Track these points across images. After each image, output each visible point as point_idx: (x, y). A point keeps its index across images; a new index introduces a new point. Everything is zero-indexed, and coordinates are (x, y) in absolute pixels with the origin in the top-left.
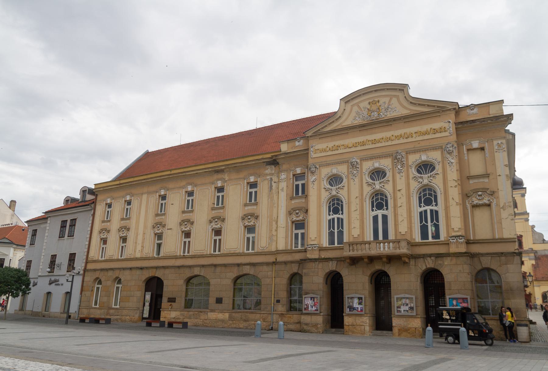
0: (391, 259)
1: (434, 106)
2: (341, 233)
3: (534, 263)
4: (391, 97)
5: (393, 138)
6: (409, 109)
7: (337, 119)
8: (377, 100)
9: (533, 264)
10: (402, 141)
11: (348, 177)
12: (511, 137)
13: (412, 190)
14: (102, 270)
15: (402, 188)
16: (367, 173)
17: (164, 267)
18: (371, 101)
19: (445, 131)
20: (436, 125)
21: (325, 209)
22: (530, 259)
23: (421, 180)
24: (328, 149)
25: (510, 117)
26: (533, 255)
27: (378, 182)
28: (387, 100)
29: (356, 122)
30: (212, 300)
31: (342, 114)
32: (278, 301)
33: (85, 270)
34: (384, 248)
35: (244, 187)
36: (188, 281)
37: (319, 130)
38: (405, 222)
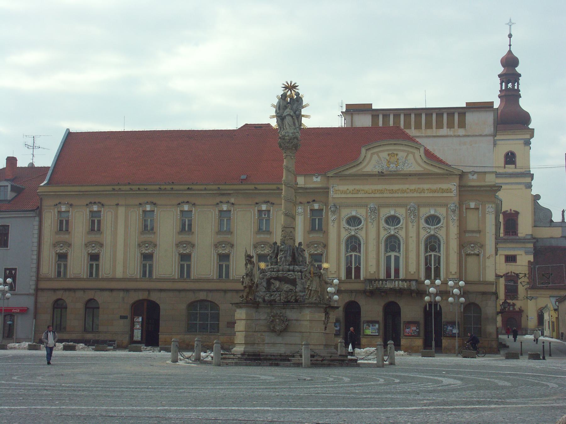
0: (400, 292)
1: (444, 169)
2: (358, 269)
3: (532, 260)
4: (409, 153)
5: (408, 191)
6: (422, 167)
7: (358, 164)
8: (395, 152)
9: (529, 262)
10: (415, 195)
11: (366, 220)
12: (499, 202)
14: (65, 290)
15: (412, 236)
16: (424, 218)
17: (161, 290)
18: (390, 152)
19: (451, 192)
20: (445, 186)
21: (343, 247)
22: (527, 253)
24: (348, 192)
26: (531, 245)
27: (393, 228)
31: (363, 160)
33: (37, 290)
34: (186, 228)
36: (192, 305)
38: (412, 263)
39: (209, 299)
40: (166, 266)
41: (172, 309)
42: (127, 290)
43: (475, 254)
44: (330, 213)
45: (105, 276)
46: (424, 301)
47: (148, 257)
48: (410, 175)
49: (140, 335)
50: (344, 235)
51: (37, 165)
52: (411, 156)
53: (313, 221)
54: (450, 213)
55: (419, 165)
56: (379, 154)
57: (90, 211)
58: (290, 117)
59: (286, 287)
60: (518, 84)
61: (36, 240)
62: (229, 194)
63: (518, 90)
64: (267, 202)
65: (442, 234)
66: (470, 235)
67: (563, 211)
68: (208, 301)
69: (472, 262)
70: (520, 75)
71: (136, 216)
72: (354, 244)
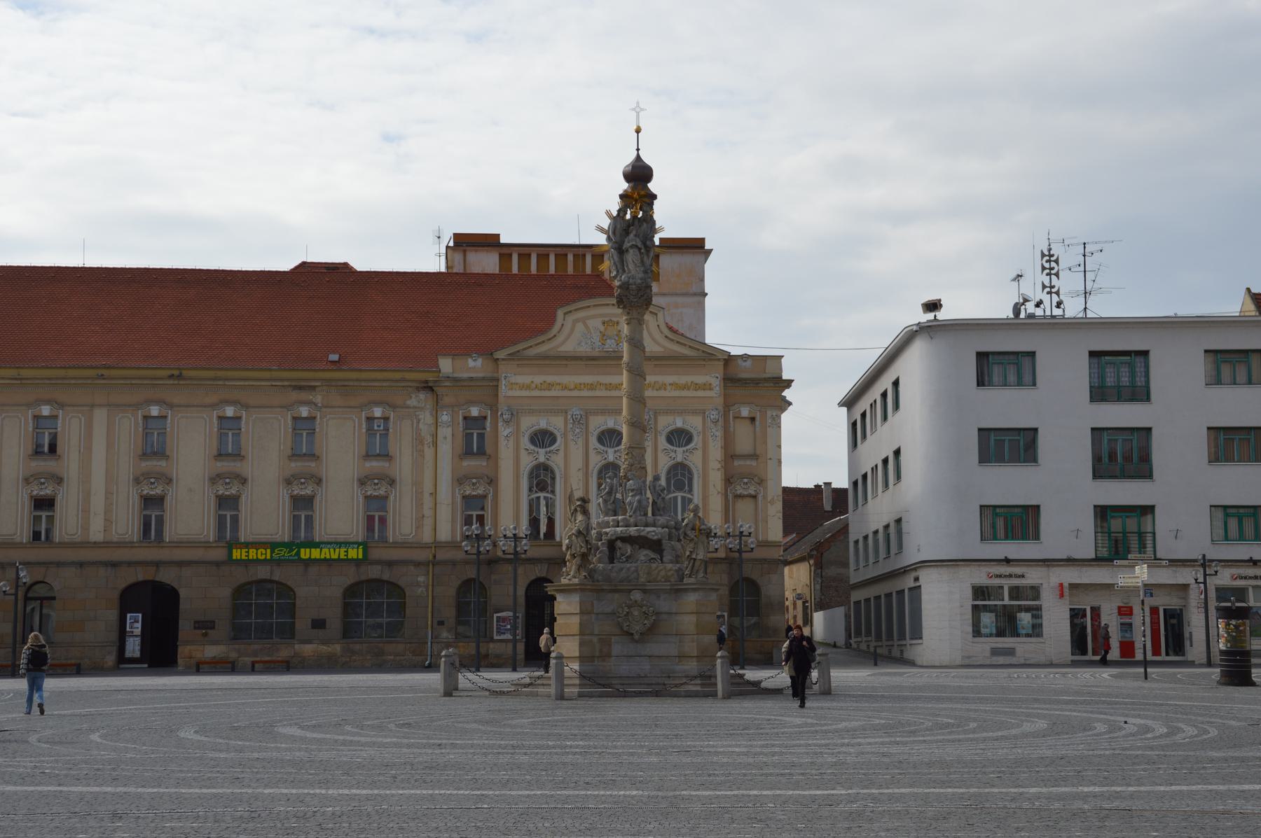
2: (160, 532)
8: (615, 319)
11: (565, 435)
13: (660, 467)
16: (596, 433)
17: (181, 564)
19: (711, 389)
20: (700, 379)
23: (673, 455)
25: (789, 383)
29: (581, 349)
30: (302, 624)
32: (441, 623)
34: (228, 448)
35: (360, 425)
39: (276, 578)
40: (190, 517)
41: (200, 596)
42: (114, 565)
44: (500, 424)
45: (67, 539)
47: (44, 504)
49: (138, 648)
50: (527, 463)
53: (468, 437)
54: (709, 423)
56: (588, 322)
57: (220, 418)
62: (313, 388)
64: (48, 402)
65: (695, 461)
66: (741, 462)
68: (271, 581)
69: (744, 507)
70: (654, 197)
71: (128, 427)
72: (542, 478)
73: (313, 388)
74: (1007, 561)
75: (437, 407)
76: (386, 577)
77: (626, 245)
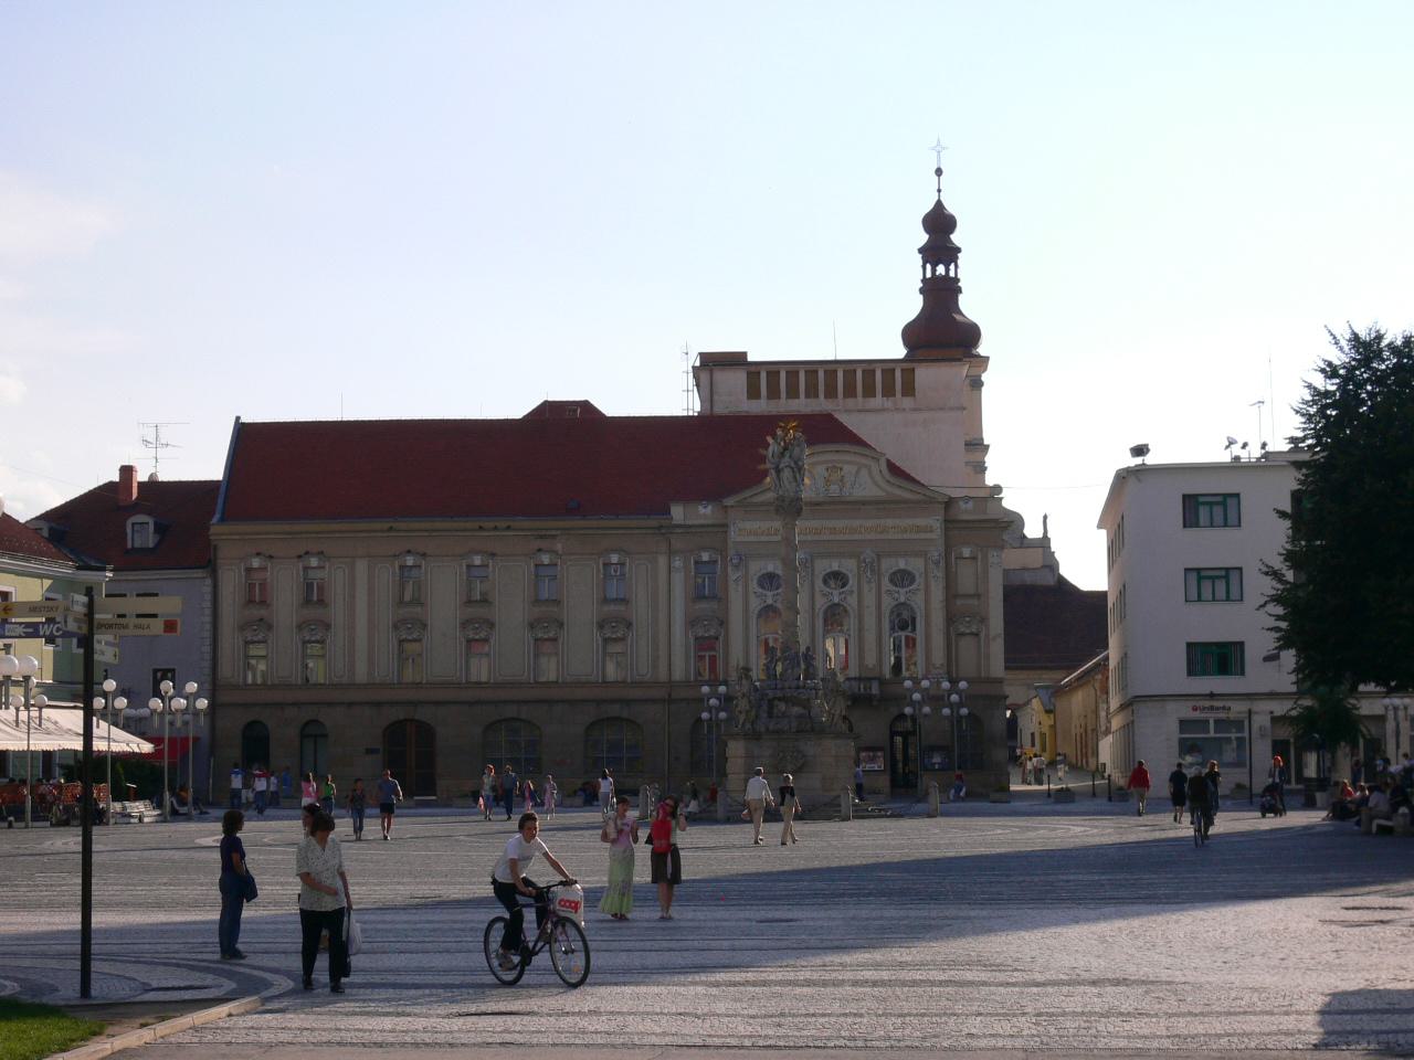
13: (883, 608)
17: (437, 703)
19: (931, 531)
20: (921, 522)
23: (896, 595)
28: (853, 469)
35: (598, 571)
37: (745, 499)
42: (378, 704)
43: (972, 634)
44: (730, 569)
46: (700, 691)
48: (864, 503)
51: (163, 477)
52: (864, 472)
55: (879, 486)
58: (789, 469)
59: (796, 710)
60: (956, 267)
61: (208, 619)
62: (554, 537)
63: (956, 280)
65: (918, 602)
67: (1045, 517)
73: (554, 537)
74: (1212, 696)
75: (671, 553)
76: (625, 715)
77: (782, 466)
